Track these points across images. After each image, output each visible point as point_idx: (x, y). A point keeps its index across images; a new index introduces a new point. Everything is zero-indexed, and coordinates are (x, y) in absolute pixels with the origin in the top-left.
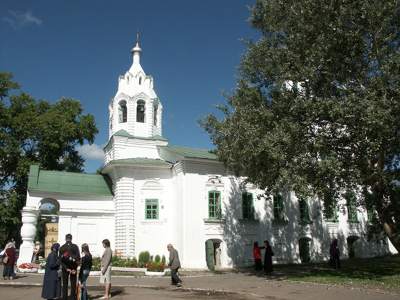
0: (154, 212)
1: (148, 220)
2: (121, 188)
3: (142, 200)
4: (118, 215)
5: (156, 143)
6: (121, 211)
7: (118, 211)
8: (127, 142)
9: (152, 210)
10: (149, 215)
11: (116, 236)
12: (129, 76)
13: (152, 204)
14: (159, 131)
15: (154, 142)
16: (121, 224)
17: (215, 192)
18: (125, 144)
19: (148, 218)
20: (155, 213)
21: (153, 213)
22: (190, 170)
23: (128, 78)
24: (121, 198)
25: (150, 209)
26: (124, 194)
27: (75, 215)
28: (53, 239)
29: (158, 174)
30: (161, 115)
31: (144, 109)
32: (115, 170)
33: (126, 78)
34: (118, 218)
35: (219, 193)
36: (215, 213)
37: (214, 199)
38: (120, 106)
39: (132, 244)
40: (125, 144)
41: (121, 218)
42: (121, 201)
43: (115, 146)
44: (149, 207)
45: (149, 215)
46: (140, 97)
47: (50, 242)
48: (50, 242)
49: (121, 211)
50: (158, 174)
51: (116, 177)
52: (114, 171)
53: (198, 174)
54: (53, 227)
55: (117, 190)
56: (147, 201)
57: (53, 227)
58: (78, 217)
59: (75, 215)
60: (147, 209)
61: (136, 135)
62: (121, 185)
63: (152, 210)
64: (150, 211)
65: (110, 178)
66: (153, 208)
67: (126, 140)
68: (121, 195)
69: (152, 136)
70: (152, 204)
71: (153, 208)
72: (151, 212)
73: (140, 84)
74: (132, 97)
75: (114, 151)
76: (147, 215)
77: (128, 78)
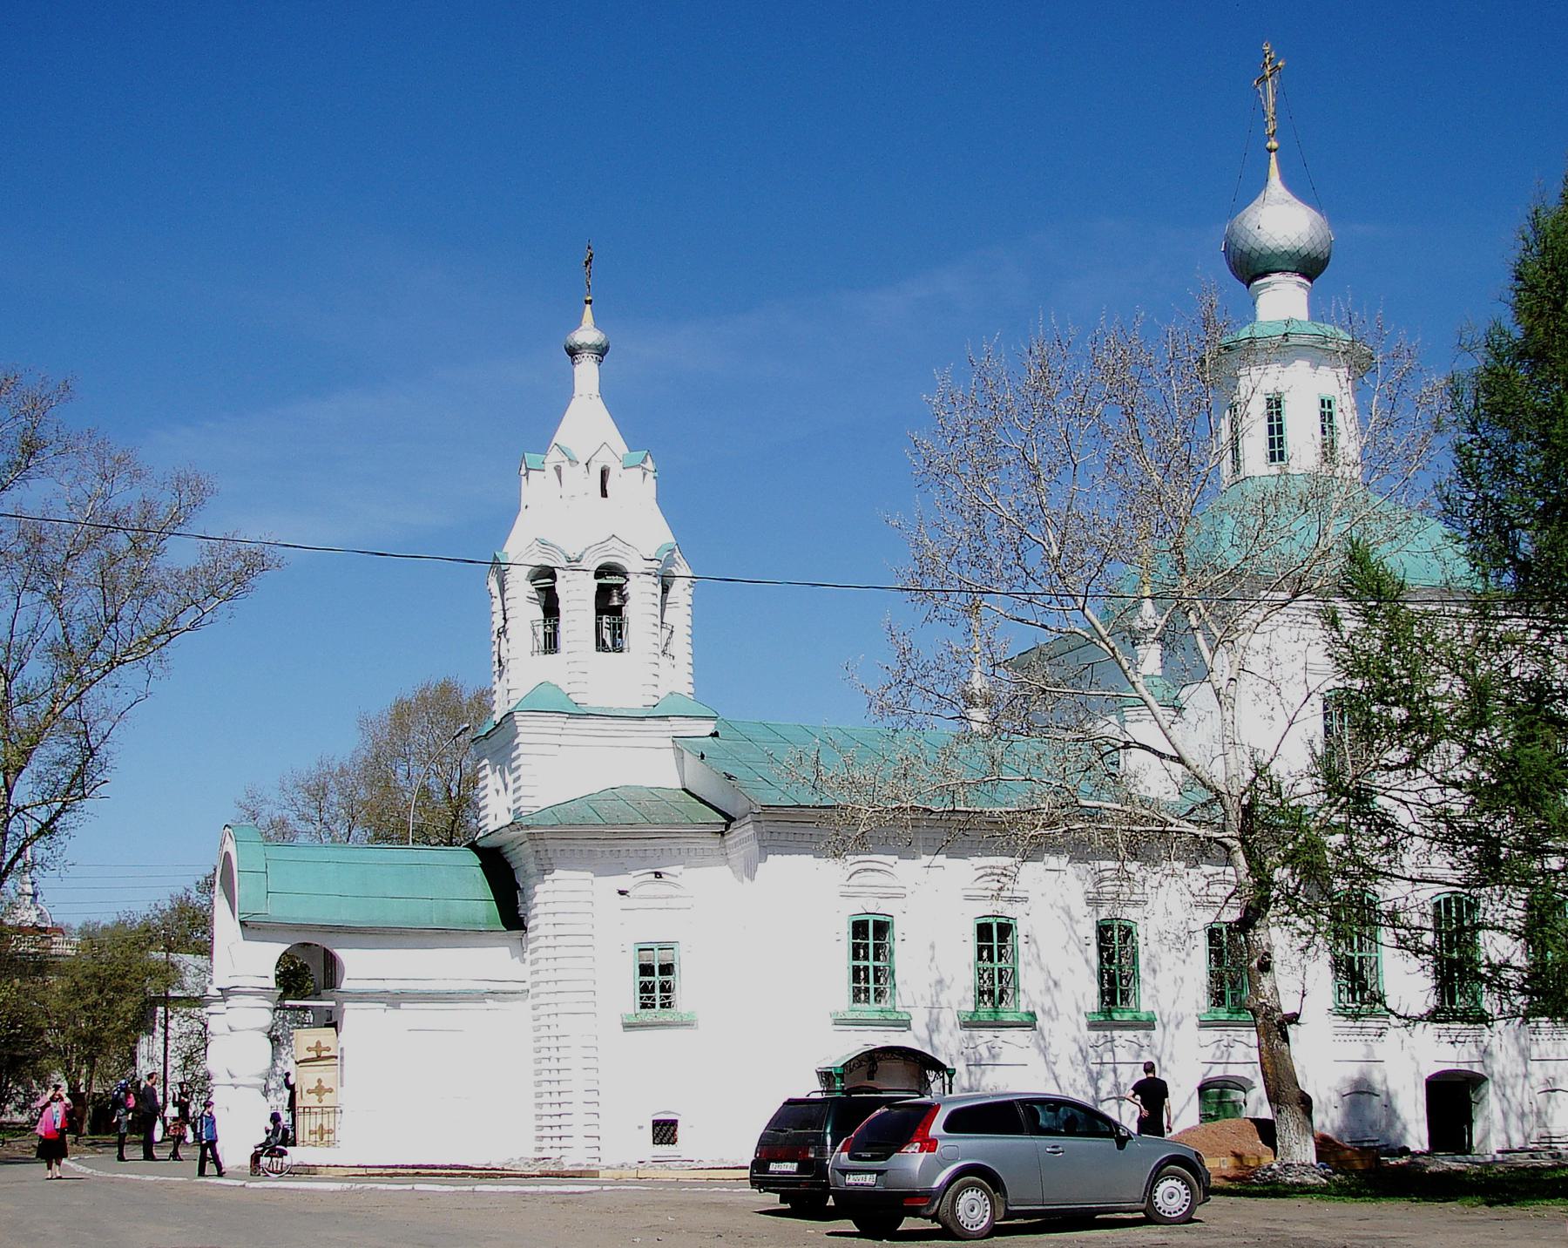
0: (665, 988)
1: (648, 1015)
2: (551, 908)
3: (623, 948)
4: (543, 999)
5: (670, 728)
6: (552, 987)
7: (543, 988)
8: (565, 732)
9: (657, 979)
10: (649, 998)
11: (539, 1117)
12: (561, 464)
13: (656, 960)
14: (678, 678)
15: (664, 725)
16: (554, 1031)
17: (871, 919)
18: (557, 740)
19: (644, 1006)
20: (669, 990)
21: (663, 989)
22: (779, 843)
23: (558, 470)
24: (551, 941)
25: (650, 979)
26: (559, 930)
27: (394, 999)
28: (319, 1081)
29: (675, 852)
30: (689, 611)
31: (624, 598)
32: (527, 844)
33: (550, 468)
34: (543, 1010)
35: (888, 919)
36: (872, 991)
37: (871, 942)
38: (533, 589)
39: (592, 1097)
40: (557, 740)
41: (552, 1009)
42: (550, 953)
43: (521, 749)
44: (646, 970)
45: (649, 998)
46: (607, 553)
47: (309, 1092)
48: (309, 1092)
49: (552, 987)
50: (675, 852)
51: (531, 867)
52: (523, 846)
53: (1308, 364)
54: (318, 1043)
55: (536, 916)
56: (640, 950)
57: (318, 1043)
58: (402, 1005)
59: (394, 999)
60: (641, 975)
61: (593, 702)
62: (549, 897)
63: (657, 979)
64: (650, 982)
65: (508, 865)
66: (661, 974)
67: (562, 725)
68: (551, 931)
69: (655, 701)
70: (657, 960)
71: (661, 974)
72: (653, 987)
73: (604, 494)
74: (577, 556)
75: (520, 788)
76: (641, 998)
77: (558, 470)
